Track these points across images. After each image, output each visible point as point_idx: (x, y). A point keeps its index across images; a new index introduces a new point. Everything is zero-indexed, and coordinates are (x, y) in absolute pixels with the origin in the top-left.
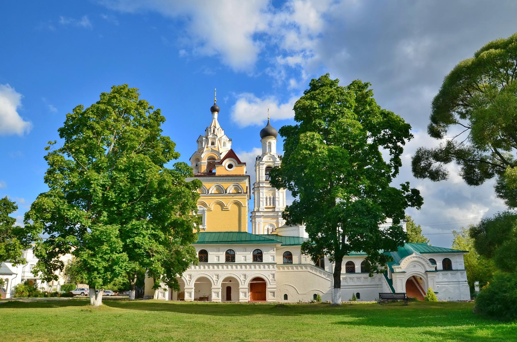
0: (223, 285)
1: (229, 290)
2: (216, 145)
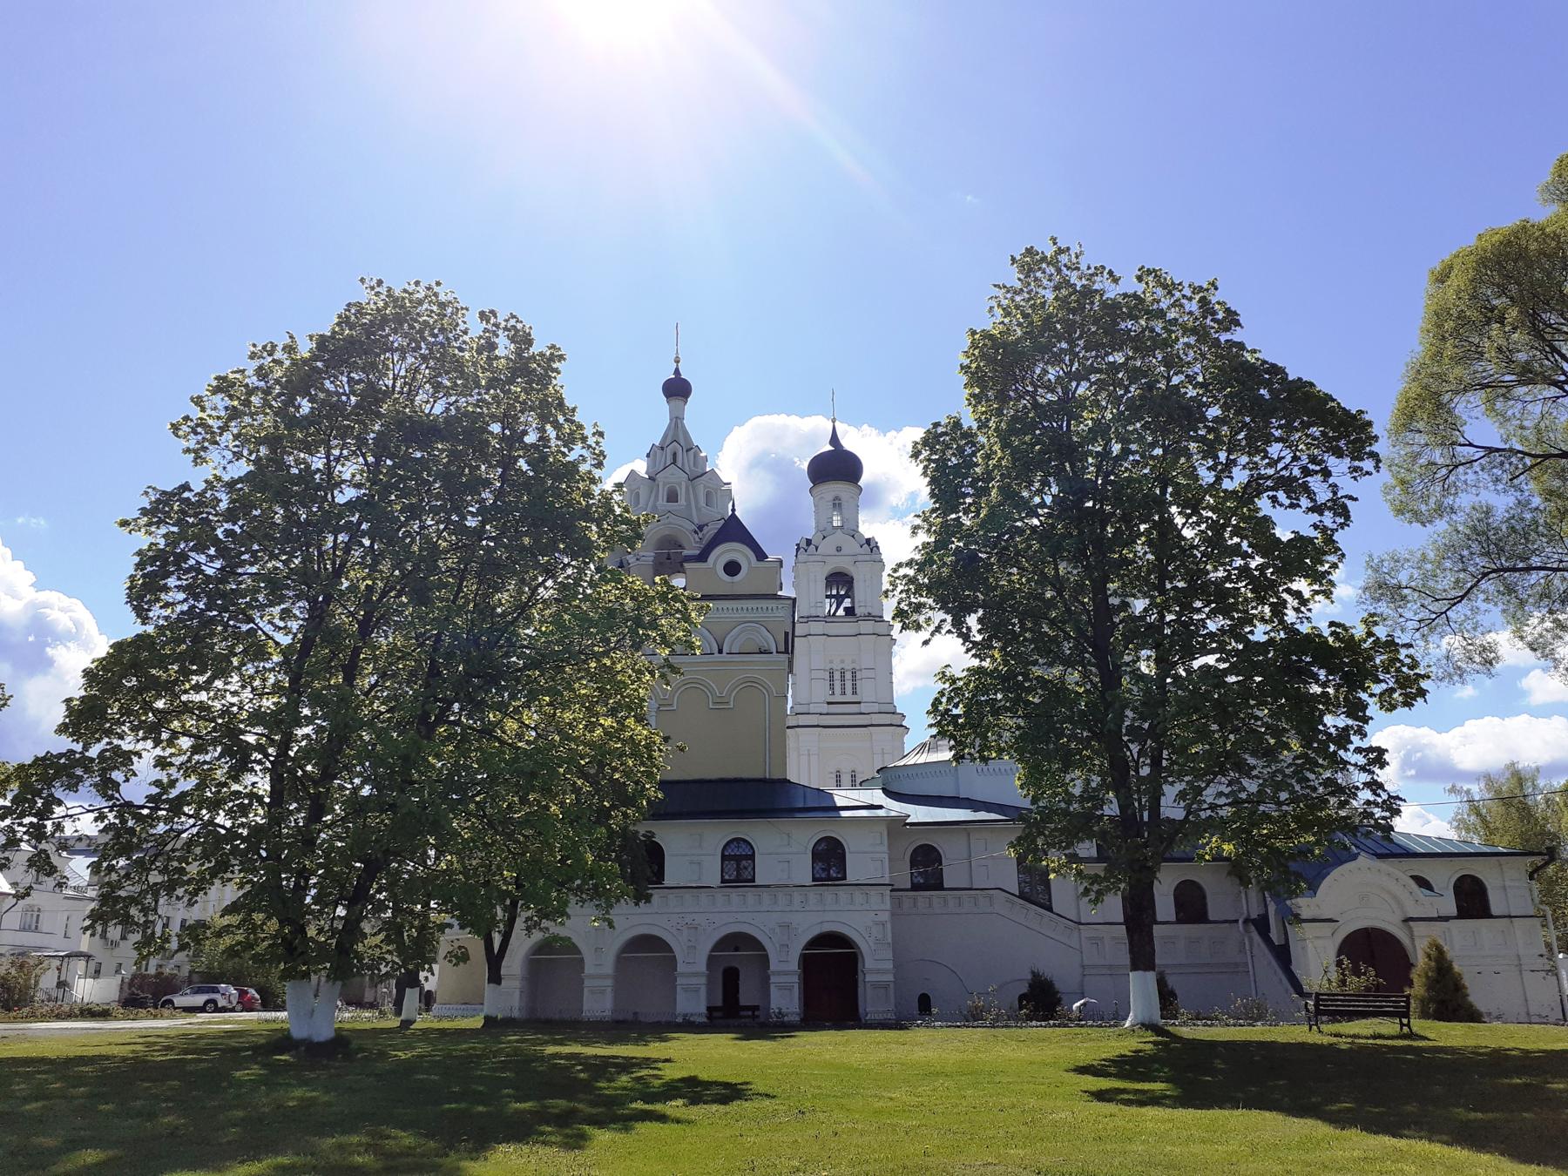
0: (711, 961)
1: (731, 979)
2: (682, 501)
